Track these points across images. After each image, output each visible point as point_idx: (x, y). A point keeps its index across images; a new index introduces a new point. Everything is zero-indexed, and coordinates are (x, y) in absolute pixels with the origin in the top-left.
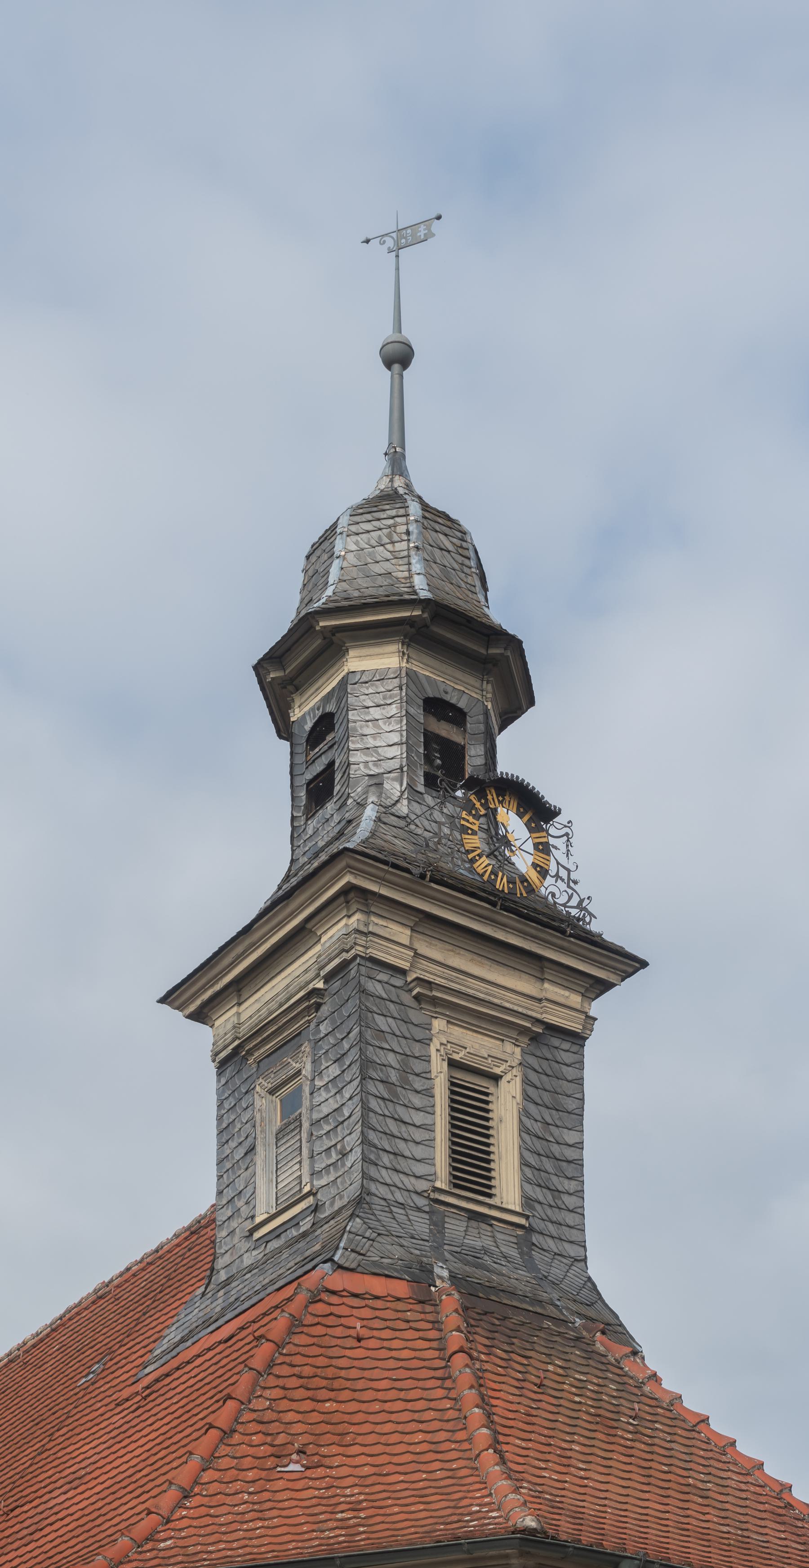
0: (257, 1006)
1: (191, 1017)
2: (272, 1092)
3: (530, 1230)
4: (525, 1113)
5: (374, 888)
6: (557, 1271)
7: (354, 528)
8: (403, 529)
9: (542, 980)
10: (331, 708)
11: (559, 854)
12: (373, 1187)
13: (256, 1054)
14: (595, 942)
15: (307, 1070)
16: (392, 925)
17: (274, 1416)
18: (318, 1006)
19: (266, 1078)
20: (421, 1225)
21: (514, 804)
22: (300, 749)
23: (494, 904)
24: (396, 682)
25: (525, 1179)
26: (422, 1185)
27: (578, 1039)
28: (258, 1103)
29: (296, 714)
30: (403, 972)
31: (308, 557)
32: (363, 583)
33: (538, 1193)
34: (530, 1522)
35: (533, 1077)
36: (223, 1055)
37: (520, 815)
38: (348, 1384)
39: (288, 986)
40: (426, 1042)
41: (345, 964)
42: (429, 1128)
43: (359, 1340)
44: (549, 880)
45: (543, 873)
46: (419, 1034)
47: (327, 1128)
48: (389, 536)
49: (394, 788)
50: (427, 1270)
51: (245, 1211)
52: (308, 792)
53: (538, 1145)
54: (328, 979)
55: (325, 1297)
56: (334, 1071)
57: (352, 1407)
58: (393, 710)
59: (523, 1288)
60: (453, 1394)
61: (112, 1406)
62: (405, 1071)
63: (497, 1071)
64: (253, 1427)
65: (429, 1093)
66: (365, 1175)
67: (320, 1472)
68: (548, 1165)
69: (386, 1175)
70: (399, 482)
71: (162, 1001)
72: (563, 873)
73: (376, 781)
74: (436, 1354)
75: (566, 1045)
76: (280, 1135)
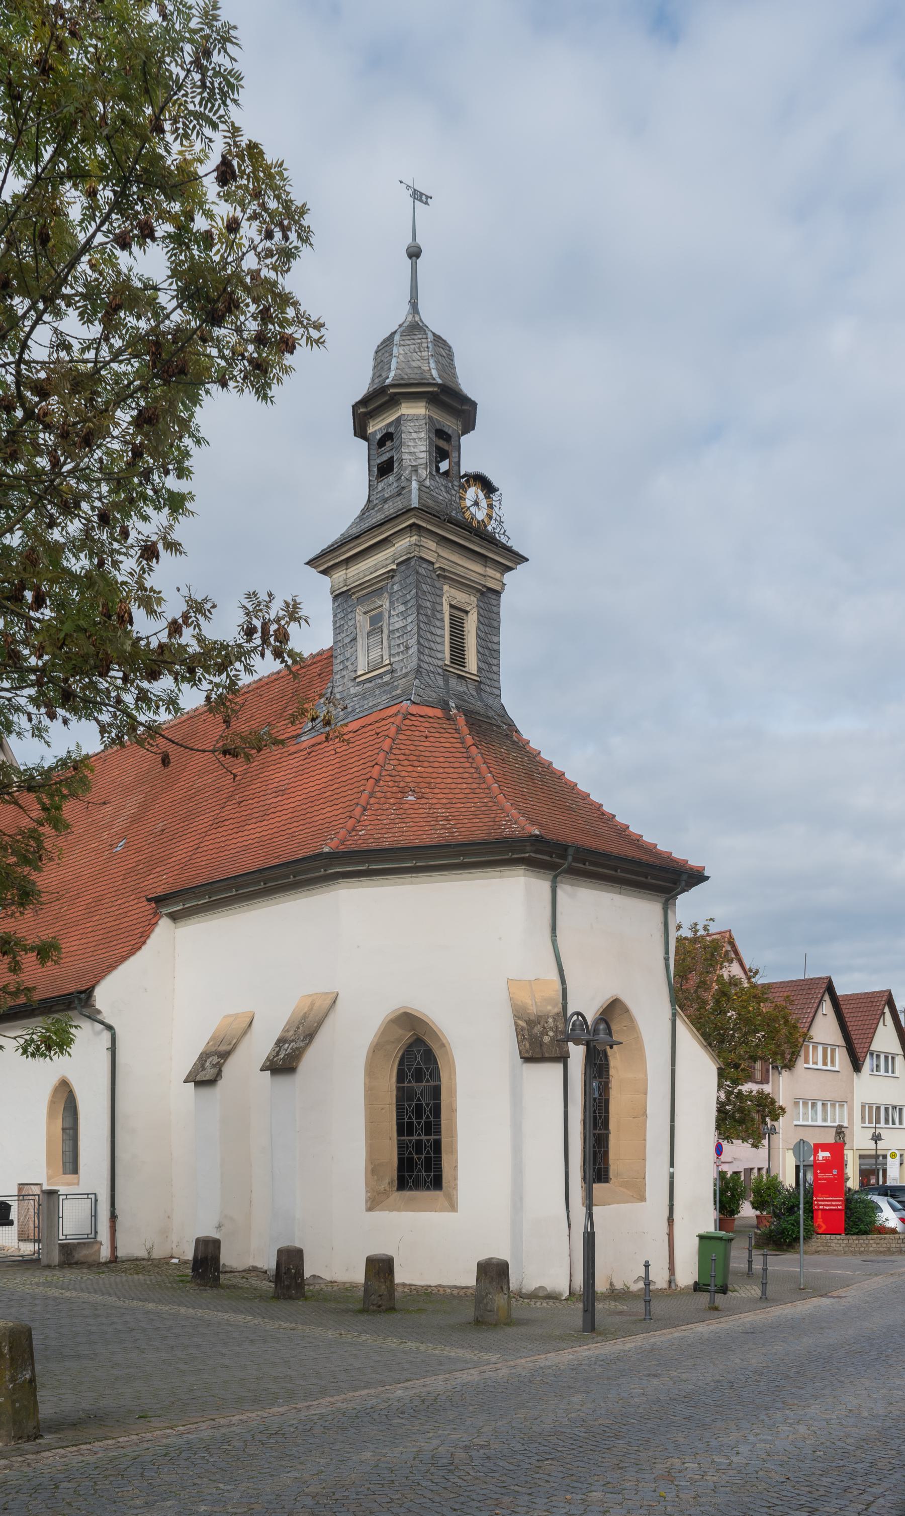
0: (357, 571)
1: (321, 572)
2: (365, 613)
3: (480, 682)
4: (478, 628)
5: (424, 525)
6: (490, 701)
7: (402, 343)
8: (425, 345)
9: (486, 566)
10: (391, 430)
11: (496, 509)
12: (422, 664)
13: (357, 595)
14: (509, 550)
15: (387, 605)
16: (429, 542)
17: (396, 773)
18: (393, 577)
19: (362, 606)
20: (441, 682)
21: (480, 486)
22: (375, 446)
23: (471, 533)
24: (424, 421)
25: (479, 659)
26: (440, 663)
27: (498, 593)
28: (358, 618)
29: (370, 430)
30: (433, 563)
31: (376, 352)
32: (409, 371)
33: (483, 666)
34: (537, 832)
35: (481, 611)
36: (337, 592)
37: (482, 491)
38: (426, 759)
39: (376, 565)
40: (441, 596)
41: (409, 559)
42: (442, 636)
43: (426, 737)
44: (493, 521)
45: (490, 518)
46: (439, 592)
47: (398, 635)
48: (419, 348)
49: (423, 473)
50: (447, 704)
51: (351, 668)
52: (378, 469)
53: (483, 643)
54: (398, 565)
55: (409, 717)
56: (402, 608)
57: (430, 770)
58: (423, 435)
59: (482, 711)
60: (474, 765)
61: (286, 754)
62: (434, 610)
63: (468, 609)
64: (388, 778)
65: (442, 620)
66: (419, 659)
67: (423, 801)
68: (487, 652)
69: (427, 659)
70: (417, 319)
71: (307, 563)
72: (498, 518)
73: (415, 469)
74: (460, 745)
75: (494, 597)
76: (369, 634)
